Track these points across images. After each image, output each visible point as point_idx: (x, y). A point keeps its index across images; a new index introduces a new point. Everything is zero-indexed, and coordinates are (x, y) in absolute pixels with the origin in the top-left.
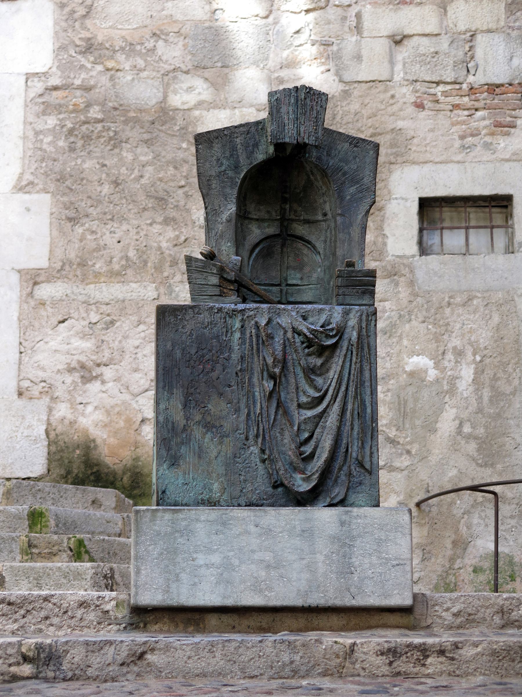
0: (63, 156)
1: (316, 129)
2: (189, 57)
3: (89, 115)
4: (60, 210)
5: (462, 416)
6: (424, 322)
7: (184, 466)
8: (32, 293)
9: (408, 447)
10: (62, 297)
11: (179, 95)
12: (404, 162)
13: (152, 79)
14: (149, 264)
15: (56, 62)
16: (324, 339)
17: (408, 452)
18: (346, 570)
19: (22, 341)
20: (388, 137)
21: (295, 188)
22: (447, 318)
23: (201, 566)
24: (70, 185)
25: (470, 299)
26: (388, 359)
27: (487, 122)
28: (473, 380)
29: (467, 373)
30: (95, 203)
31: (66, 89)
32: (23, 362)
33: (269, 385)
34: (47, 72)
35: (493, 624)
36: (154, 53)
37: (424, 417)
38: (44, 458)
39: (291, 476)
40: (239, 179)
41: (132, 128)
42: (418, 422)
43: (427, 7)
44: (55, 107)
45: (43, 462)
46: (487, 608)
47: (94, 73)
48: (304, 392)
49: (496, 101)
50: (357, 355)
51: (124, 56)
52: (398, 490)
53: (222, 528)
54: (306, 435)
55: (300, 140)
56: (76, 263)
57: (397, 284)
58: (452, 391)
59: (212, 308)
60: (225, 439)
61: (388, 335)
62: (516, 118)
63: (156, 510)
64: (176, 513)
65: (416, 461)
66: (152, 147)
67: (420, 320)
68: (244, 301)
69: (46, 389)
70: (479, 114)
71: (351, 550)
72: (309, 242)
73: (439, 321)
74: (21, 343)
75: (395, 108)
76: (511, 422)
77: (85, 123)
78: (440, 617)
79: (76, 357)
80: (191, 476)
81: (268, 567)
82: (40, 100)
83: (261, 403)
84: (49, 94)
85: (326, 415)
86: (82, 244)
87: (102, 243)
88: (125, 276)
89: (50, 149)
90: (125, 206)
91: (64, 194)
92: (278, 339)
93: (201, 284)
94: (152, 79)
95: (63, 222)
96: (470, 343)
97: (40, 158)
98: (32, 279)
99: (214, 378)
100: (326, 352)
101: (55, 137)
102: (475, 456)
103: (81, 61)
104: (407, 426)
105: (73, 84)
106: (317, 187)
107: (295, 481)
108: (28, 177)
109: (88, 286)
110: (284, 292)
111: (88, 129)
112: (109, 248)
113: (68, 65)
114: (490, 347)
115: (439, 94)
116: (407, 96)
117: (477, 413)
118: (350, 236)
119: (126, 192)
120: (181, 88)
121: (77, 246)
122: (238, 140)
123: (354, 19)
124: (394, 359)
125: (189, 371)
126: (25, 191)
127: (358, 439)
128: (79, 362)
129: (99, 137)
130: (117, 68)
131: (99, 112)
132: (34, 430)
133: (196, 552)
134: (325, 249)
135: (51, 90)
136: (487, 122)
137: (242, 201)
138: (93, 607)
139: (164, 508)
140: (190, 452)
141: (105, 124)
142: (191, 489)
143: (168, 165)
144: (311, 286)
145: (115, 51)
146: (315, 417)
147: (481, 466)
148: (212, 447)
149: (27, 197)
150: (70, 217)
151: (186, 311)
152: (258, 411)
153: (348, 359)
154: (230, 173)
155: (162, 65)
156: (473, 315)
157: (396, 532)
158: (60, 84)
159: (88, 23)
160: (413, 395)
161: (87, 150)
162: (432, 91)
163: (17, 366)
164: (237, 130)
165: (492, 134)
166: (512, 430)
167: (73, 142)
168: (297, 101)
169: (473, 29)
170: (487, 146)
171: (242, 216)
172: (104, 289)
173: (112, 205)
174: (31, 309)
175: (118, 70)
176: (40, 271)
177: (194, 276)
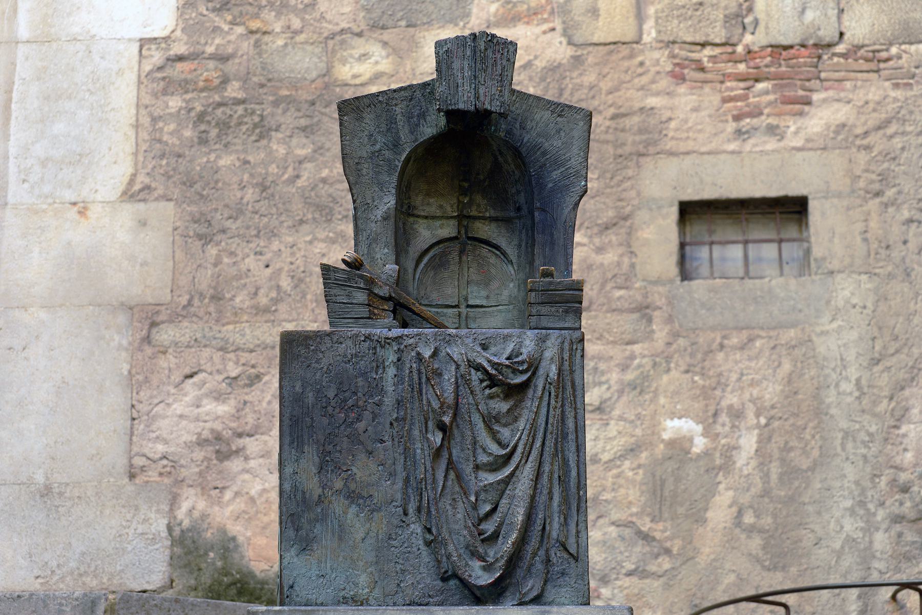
0: (190, 151)
1: (501, 91)
2: (362, 14)
3: (226, 94)
4: (187, 224)
5: (741, 501)
6: (687, 372)
7: (319, 552)
8: (148, 337)
9: (668, 544)
10: (189, 342)
11: (348, 66)
12: (658, 153)
13: (312, 44)
14: (309, 297)
15: (180, 22)
16: (511, 375)
17: (668, 551)
19: (134, 403)
20: (636, 119)
21: (478, 174)
22: (720, 366)
24: (199, 189)
25: (751, 340)
26: (639, 423)
27: (771, 97)
28: (757, 451)
29: (749, 442)
30: (235, 214)
31: (194, 59)
32: (136, 432)
33: (437, 438)
34: (169, 37)
36: (313, 9)
37: (688, 503)
38: (165, 564)
39: (467, 564)
41: (285, 111)
42: (681, 510)
44: (180, 85)
45: (164, 569)
47: (232, 38)
48: (484, 449)
50: (557, 396)
51: (273, 14)
52: (654, 603)
54: (488, 508)
56: (208, 296)
57: (650, 320)
58: (727, 466)
59: (357, 336)
61: (638, 390)
62: (811, 91)
63: (280, 611)
65: (678, 564)
66: (312, 137)
67: (683, 368)
68: (405, 325)
69: (168, 469)
70: (761, 86)
72: (497, 247)
73: (709, 369)
74: (133, 406)
75: (644, 80)
76: (810, 508)
77: (220, 105)
79: (208, 425)
80: (329, 565)
82: (159, 75)
84: (172, 66)
85: (514, 479)
86: (217, 269)
87: (243, 267)
88: (276, 314)
90: (275, 217)
91: (191, 202)
92: (449, 375)
94: (312, 44)
95: (190, 240)
96: (753, 401)
97: (159, 153)
98: (148, 320)
99: (361, 431)
100: (516, 392)
101: (179, 125)
102: (760, 555)
103: (214, 22)
104: (666, 515)
105: (203, 53)
106: (508, 173)
107: (473, 571)
108: (142, 179)
109: (225, 328)
110: (463, 316)
111: (224, 113)
112: (254, 276)
113: (198, 26)
114: (779, 406)
115: (705, 59)
116: (662, 63)
117: (762, 496)
118: (552, 238)
119: (277, 198)
120: (351, 56)
121: (209, 272)
124: (647, 423)
125: (325, 421)
126: (139, 197)
127: (559, 512)
128: (212, 431)
130: (264, 29)
131: (240, 89)
132: (151, 525)
134: (519, 257)
135: (174, 61)
136: (771, 97)
137: (404, 191)
139: (291, 608)
141: (248, 107)
142: (329, 583)
143: (333, 161)
144: (500, 307)
145: (260, 7)
146: (499, 482)
147: (769, 570)
149: (142, 206)
150: (202, 231)
153: (545, 403)
154: (387, 154)
155: (325, 25)
156: (755, 362)
158: (187, 52)
160: (673, 471)
161: (223, 142)
163: (127, 438)
164: (396, 95)
165: (779, 115)
166: (811, 519)
167: (204, 132)
168: (475, 52)
170: (772, 130)
171: (405, 213)
172: (248, 331)
173: (257, 216)
174: (147, 359)
175: (265, 33)
176: (158, 308)
177: (333, 292)
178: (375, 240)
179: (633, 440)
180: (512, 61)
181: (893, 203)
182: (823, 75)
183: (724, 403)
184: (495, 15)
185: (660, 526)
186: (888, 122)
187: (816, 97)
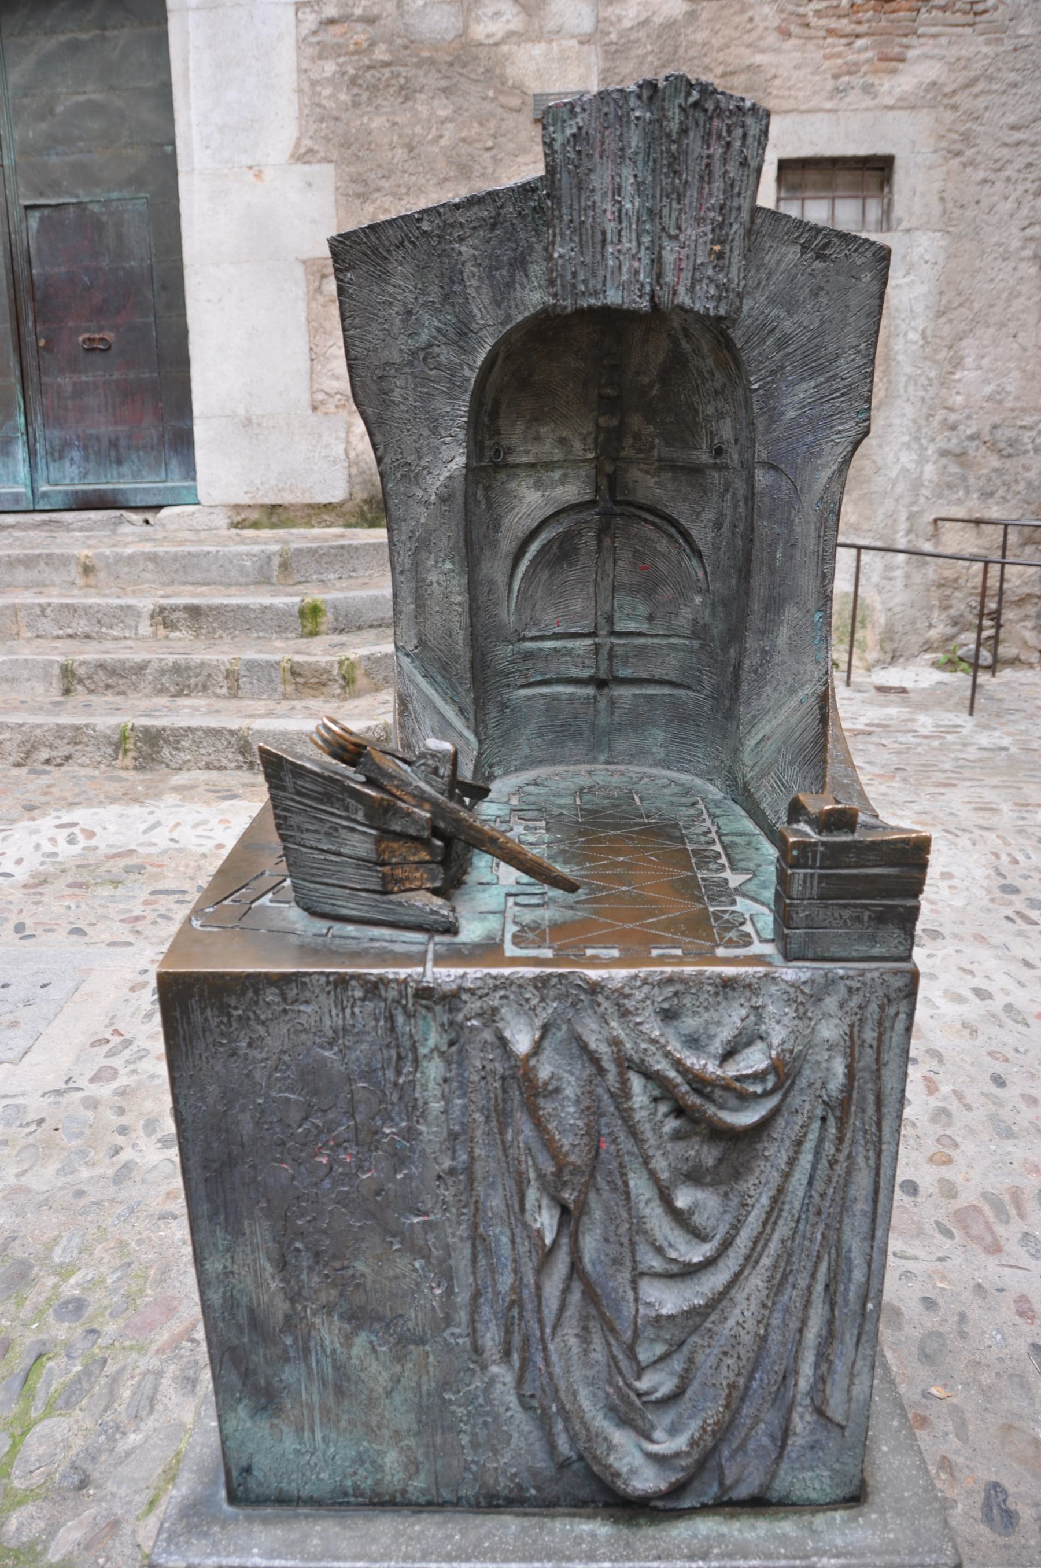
1: (720, 256)
7: (296, 1412)
16: (733, 1102)
21: (638, 373)
27: (869, 54)
40: (471, 369)
49: (883, 23)
60: (412, 1347)
70: (860, 43)
75: (754, 35)
77: (370, 68)
82: (314, 39)
85: (724, 1303)
89: (329, 104)
106: (700, 373)
108: (307, 143)
110: (604, 652)
129: (388, 86)
134: (716, 547)
136: (869, 54)
144: (674, 641)
149: (307, 168)
151: (256, 992)
153: (809, 1146)
154: (445, 354)
164: (461, 217)
165: (875, 72)
170: (868, 89)
180: (753, 164)
181: (972, 163)
182: (921, 31)
186: (975, 81)
187: (911, 54)
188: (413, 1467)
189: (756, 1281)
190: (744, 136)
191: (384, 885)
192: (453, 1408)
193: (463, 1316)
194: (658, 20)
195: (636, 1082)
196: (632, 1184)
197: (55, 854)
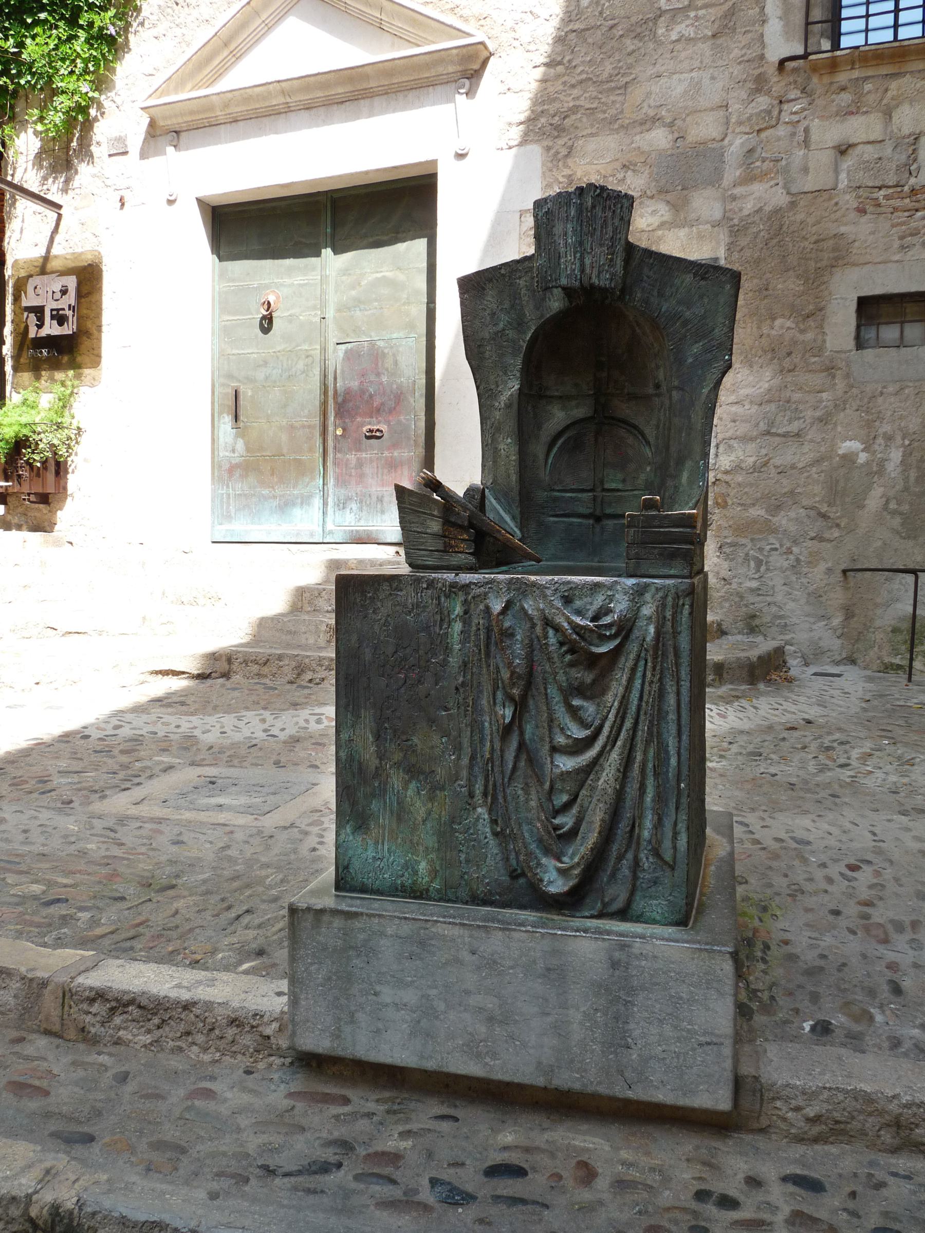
1: (611, 260)
6: (857, 410)
7: (376, 831)
9: (838, 521)
16: (596, 641)
17: (838, 525)
18: (618, 1041)
20: (831, 243)
23: (387, 1005)
29: (896, 455)
35: (879, 1142)
40: (524, 341)
42: (847, 500)
43: (872, 115)
46: (870, 1114)
50: (654, 669)
53: (418, 951)
54: (565, 798)
55: (586, 282)
57: (834, 377)
58: (881, 471)
60: (438, 792)
64: (351, 918)
67: (855, 408)
70: (919, 214)
71: (627, 1010)
72: (635, 427)
75: (838, 214)
78: (784, 1119)
80: (386, 847)
81: (491, 1019)
83: (491, 741)
85: (597, 768)
93: (419, 532)
96: (900, 429)
110: (599, 500)
122: (522, 282)
123: (802, 133)
125: (383, 682)
133: (379, 982)
134: (657, 438)
138: (247, 1029)
140: (385, 809)
148: (418, 804)
152: (487, 755)
153: (639, 674)
154: (511, 334)
157: (708, 988)
159: (570, 161)
162: (875, 195)
168: (581, 211)
169: (918, 132)
178: (498, 430)
179: (818, 455)
180: (626, 219)
183: (881, 431)
184: (739, 177)
185: (834, 509)
188: (434, 873)
189: (615, 756)
190: (622, 207)
191: (445, 547)
192: (457, 834)
193: (464, 773)
194: (767, 209)
195: (551, 632)
196: (549, 691)
197: (307, 728)
